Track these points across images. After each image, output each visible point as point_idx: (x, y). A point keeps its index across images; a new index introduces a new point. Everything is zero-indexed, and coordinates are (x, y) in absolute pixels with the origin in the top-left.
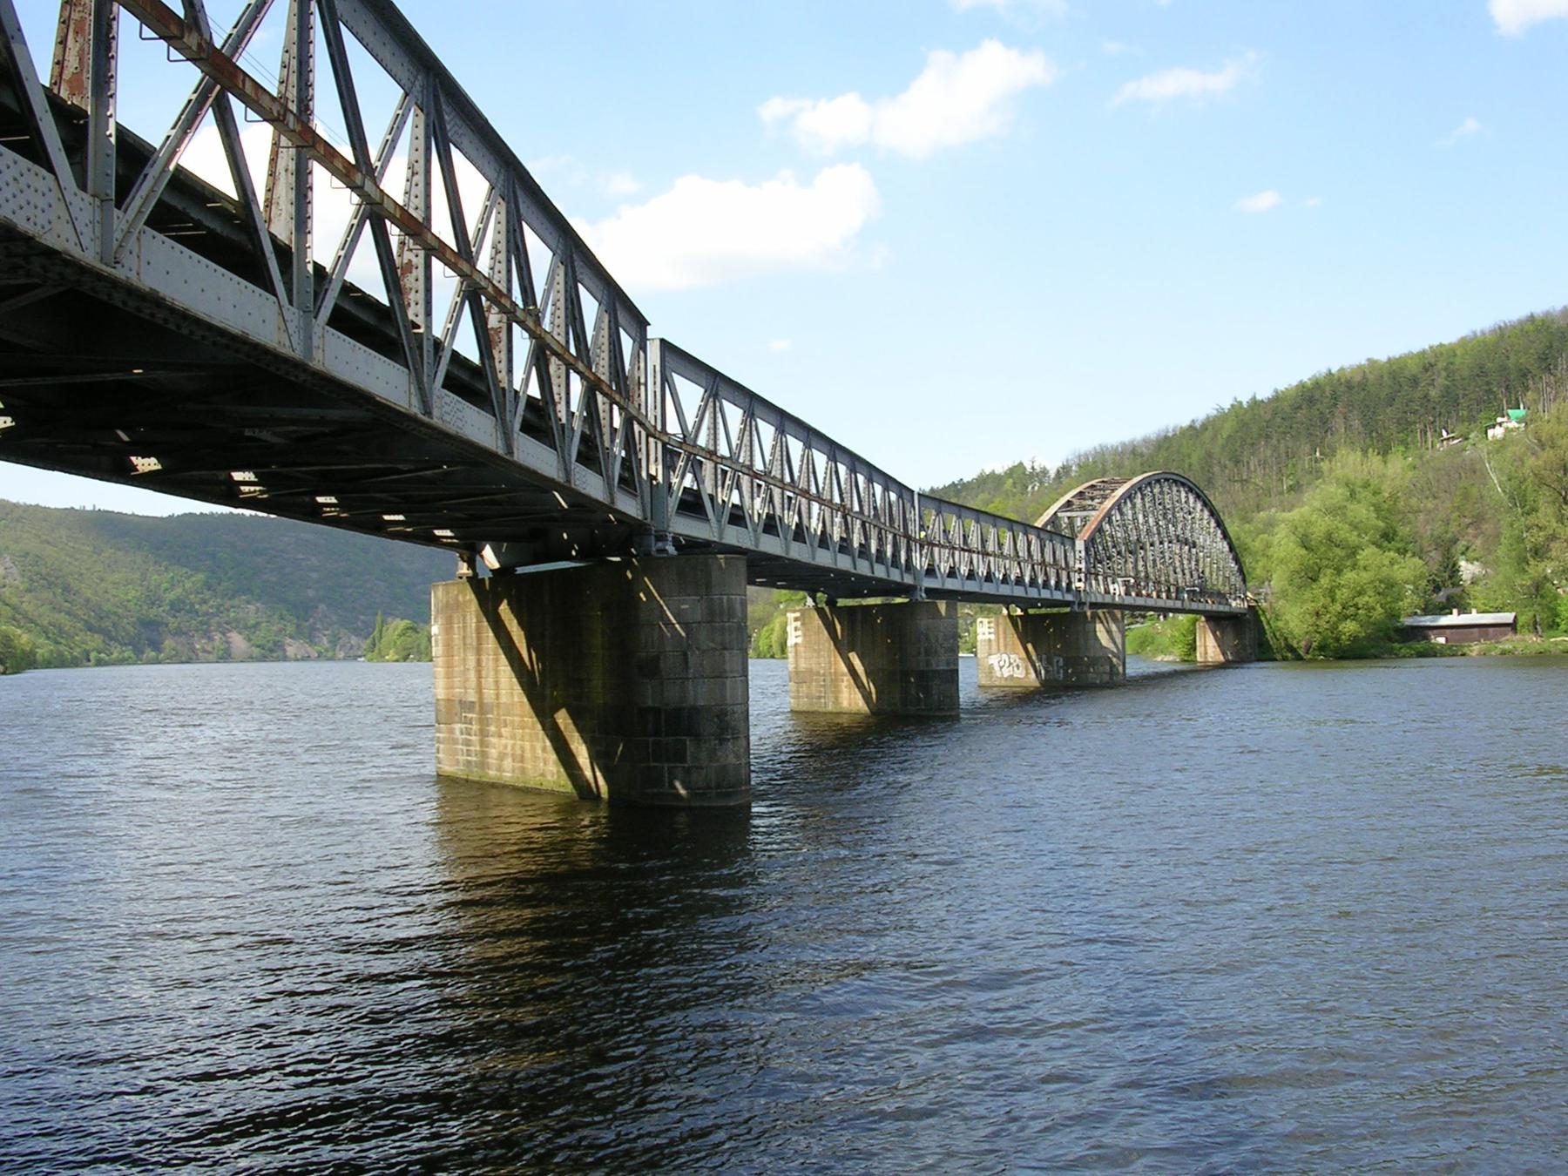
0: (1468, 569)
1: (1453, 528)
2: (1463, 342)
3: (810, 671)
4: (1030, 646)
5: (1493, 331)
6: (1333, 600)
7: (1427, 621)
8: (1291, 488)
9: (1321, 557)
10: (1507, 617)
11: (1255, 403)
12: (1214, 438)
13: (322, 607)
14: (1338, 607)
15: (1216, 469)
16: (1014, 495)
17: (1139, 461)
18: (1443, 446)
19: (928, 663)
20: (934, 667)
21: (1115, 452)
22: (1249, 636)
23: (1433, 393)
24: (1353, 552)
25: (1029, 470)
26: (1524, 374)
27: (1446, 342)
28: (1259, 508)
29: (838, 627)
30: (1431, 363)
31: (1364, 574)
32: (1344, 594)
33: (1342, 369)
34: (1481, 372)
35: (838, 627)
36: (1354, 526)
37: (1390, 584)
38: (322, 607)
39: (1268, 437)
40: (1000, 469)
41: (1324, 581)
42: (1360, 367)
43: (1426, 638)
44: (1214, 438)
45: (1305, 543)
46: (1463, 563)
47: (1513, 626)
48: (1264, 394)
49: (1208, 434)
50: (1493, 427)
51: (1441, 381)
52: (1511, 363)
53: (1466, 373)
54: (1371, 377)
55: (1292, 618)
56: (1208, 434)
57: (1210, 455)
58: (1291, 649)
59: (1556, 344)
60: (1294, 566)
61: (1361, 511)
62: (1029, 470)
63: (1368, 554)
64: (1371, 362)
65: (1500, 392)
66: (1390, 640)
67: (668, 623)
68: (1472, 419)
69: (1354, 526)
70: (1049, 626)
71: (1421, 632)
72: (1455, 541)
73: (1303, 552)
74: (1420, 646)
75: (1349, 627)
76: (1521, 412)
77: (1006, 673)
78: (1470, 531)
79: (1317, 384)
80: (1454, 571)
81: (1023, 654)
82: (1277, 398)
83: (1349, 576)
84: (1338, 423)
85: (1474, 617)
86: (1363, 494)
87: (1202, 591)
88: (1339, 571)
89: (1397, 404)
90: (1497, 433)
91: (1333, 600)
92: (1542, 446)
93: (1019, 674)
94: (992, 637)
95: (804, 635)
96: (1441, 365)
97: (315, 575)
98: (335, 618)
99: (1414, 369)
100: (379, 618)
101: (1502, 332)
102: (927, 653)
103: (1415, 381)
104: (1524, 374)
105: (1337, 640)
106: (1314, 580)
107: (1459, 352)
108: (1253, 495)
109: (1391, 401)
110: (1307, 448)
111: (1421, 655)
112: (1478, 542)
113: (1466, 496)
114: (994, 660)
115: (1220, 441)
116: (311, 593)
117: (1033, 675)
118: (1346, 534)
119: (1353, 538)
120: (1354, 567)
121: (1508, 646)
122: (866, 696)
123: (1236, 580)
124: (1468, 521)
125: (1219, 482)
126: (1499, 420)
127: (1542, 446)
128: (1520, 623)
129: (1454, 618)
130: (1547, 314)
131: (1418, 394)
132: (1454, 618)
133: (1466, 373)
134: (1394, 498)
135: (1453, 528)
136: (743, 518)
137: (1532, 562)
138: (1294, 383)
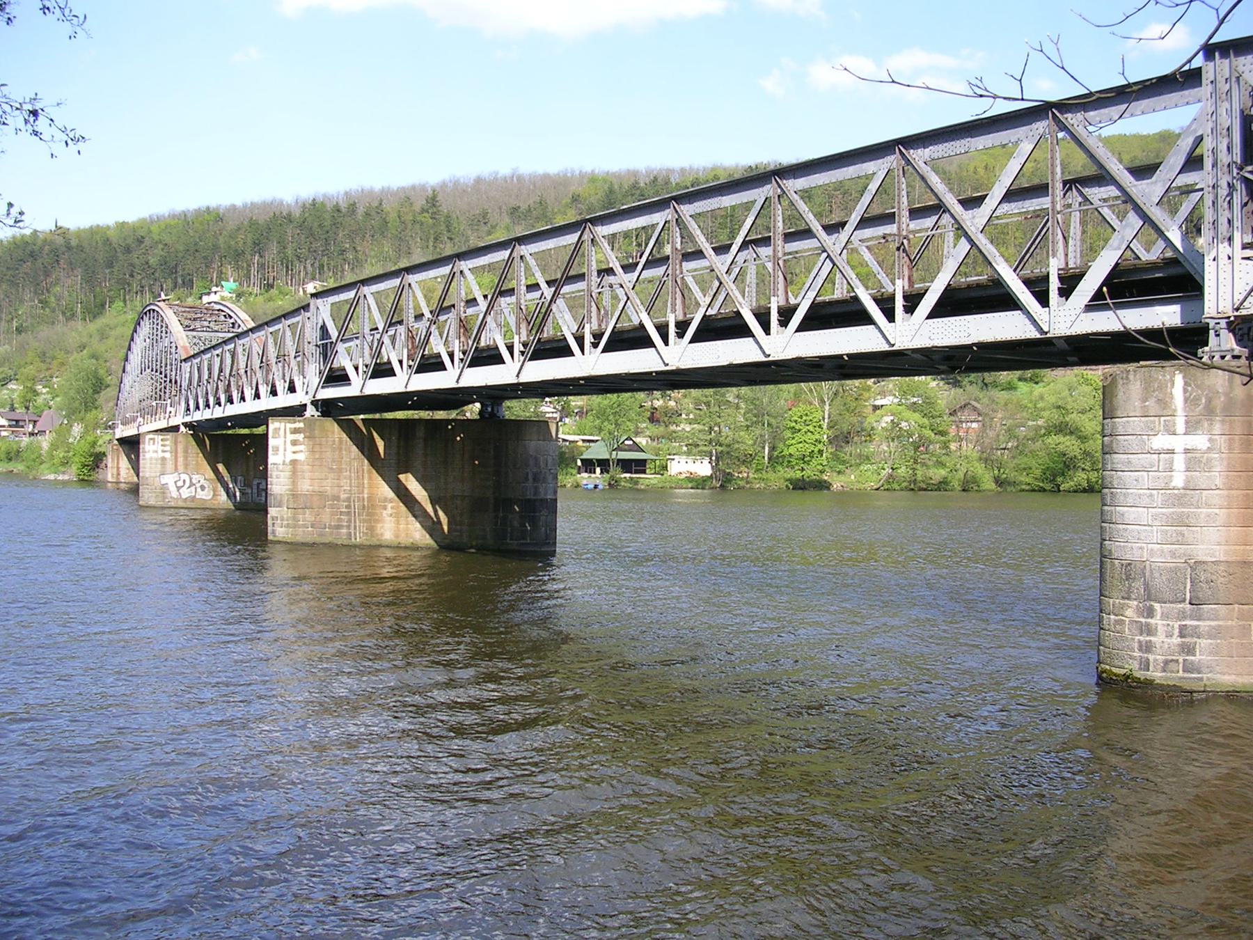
3: (321, 495)
4: (221, 467)
19: (536, 493)
20: (542, 496)
29: (380, 444)
35: (380, 444)
50: (209, 294)
70: (248, 448)
77: (186, 493)
81: (212, 475)
93: (201, 495)
94: (168, 455)
95: (312, 451)
102: (535, 479)
103: (128, 250)
114: (169, 480)
117: (223, 496)
122: (432, 527)
126: (214, 289)
136: (701, 252)
138: (710, 165)
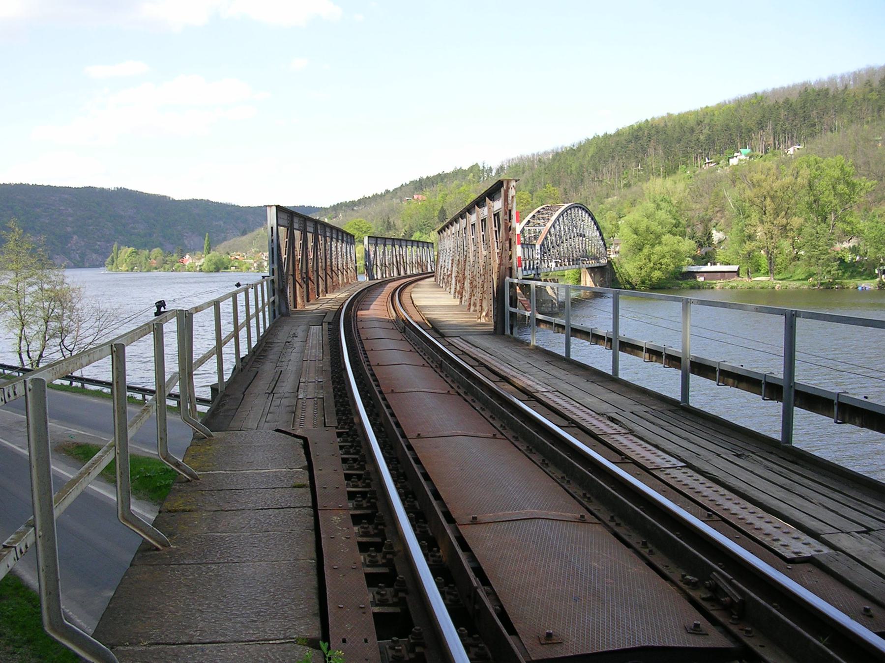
0: (717, 236)
1: (710, 213)
2: (719, 107)
5: (735, 101)
6: (650, 261)
7: (695, 269)
8: (625, 185)
9: (644, 240)
10: (734, 268)
11: (606, 137)
12: (584, 156)
13: (75, 237)
14: (652, 265)
15: (586, 174)
16: (474, 182)
17: (543, 167)
18: (706, 167)
21: (528, 159)
22: (607, 276)
23: (702, 137)
24: (658, 237)
25: (481, 168)
26: (750, 131)
27: (709, 105)
28: (608, 196)
30: (703, 118)
31: (665, 247)
32: (654, 258)
33: (653, 119)
34: (727, 128)
36: (660, 223)
37: (678, 252)
38: (75, 237)
39: (613, 158)
40: (466, 167)
41: (646, 251)
42: (663, 118)
43: (695, 278)
44: (584, 156)
45: (636, 232)
46: (714, 232)
47: (737, 273)
48: (612, 131)
49: (581, 153)
51: (706, 131)
52: (742, 124)
53: (719, 128)
54: (669, 124)
55: (629, 268)
56: (581, 153)
57: (582, 166)
58: (630, 283)
59: (767, 115)
60: (631, 242)
61: (662, 215)
62: (481, 168)
63: (667, 238)
64: (669, 115)
65: (738, 140)
66: (678, 279)
67: (774, 607)
68: (721, 152)
69: (660, 223)
71: (692, 275)
72: (710, 220)
73: (636, 236)
74: (691, 282)
75: (657, 274)
76: (748, 151)
78: (718, 214)
79: (640, 128)
80: (709, 236)
82: (618, 134)
83: (658, 248)
84: (651, 151)
85: (719, 268)
86: (663, 205)
87: (586, 256)
88: (653, 246)
89: (682, 143)
90: (734, 162)
91: (650, 261)
92: (754, 186)
96: (707, 121)
97: (70, 219)
98: (83, 244)
99: (692, 122)
100: (115, 246)
101: (740, 103)
103: (692, 130)
104: (750, 131)
105: (650, 280)
106: (640, 250)
107: (716, 113)
108: (605, 188)
109: (679, 140)
110: (634, 164)
111: (692, 288)
112: (722, 221)
113: (717, 195)
115: (587, 158)
116: (69, 229)
118: (655, 227)
119: (659, 229)
120: (660, 243)
121: (734, 284)
123: (602, 250)
124: (718, 209)
125: (586, 182)
126: (736, 154)
127: (754, 186)
128: (741, 272)
129: (709, 268)
130: (764, 92)
131: (694, 138)
132: (709, 268)
133: (719, 128)
134: (680, 203)
135: (710, 213)
137: (748, 242)
